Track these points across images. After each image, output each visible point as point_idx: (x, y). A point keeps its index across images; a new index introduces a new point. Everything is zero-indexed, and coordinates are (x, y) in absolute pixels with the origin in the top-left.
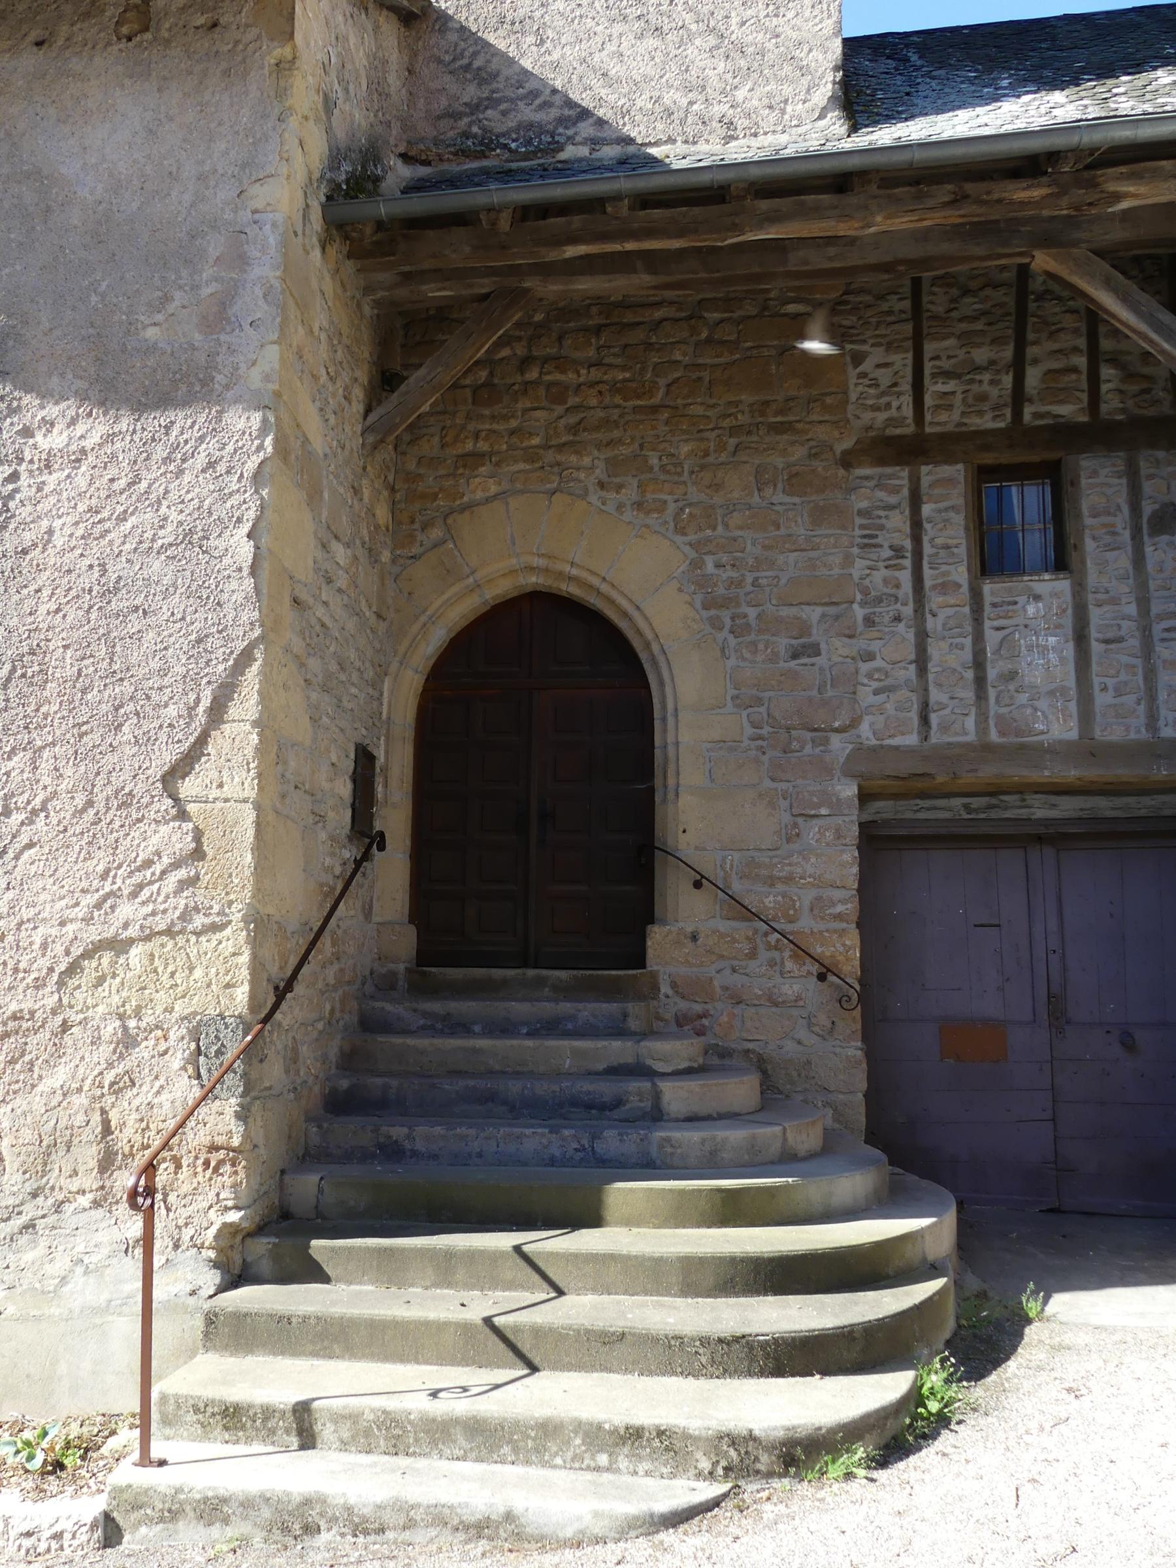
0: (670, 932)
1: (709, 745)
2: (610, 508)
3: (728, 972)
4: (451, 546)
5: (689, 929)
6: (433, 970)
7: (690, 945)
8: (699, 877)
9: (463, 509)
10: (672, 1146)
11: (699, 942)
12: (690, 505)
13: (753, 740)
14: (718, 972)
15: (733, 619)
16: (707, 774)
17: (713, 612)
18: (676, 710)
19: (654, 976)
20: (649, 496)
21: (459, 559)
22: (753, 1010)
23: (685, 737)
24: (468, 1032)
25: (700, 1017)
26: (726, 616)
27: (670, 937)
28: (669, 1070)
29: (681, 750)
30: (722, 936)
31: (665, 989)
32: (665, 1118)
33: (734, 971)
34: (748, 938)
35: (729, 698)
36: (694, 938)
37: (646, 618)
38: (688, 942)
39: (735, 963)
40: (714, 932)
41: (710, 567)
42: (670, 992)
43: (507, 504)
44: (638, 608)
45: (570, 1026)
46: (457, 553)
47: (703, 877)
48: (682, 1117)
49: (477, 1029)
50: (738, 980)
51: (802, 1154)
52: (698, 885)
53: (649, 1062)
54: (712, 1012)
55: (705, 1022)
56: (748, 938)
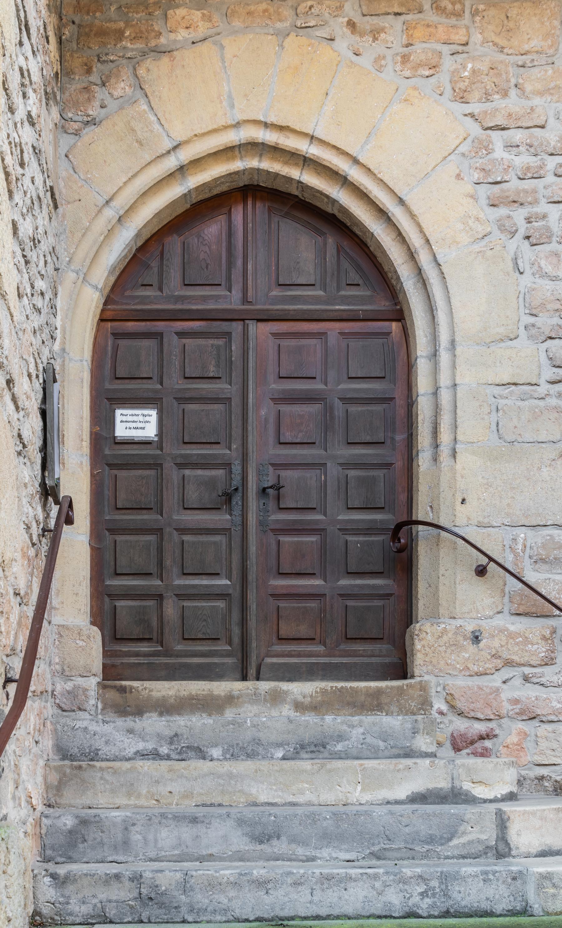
0: (445, 631)
1: (497, 391)
2: (366, 61)
3: (518, 681)
4: (145, 107)
5: (470, 627)
6: (135, 684)
7: (472, 648)
8: (485, 560)
9: (159, 52)
10: (554, 886)
11: (482, 644)
12: (474, 59)
13: (553, 383)
14: (504, 682)
15: (528, 220)
16: (494, 427)
17: (503, 211)
18: (453, 343)
19: (423, 687)
20: (418, 47)
21: (157, 126)
22: (550, 727)
23: (467, 377)
24: (204, 758)
25: (482, 738)
26: (519, 215)
27: (445, 638)
28: (491, 796)
29: (459, 395)
30: (511, 636)
31: (439, 704)
32: (513, 853)
33: (526, 679)
34: (544, 638)
35: (522, 328)
36: (476, 638)
37: (412, 216)
38: (467, 643)
39: (527, 670)
40: (501, 631)
41: (499, 153)
42: (444, 708)
43: (222, 47)
44: (401, 202)
45: (339, 747)
46: (153, 118)
47: (491, 559)
48: (534, 851)
49: (216, 752)
50: (530, 693)
51: (498, 913)
52: (481, 571)
53: (467, 786)
54: (497, 732)
55: (488, 743)
56: (544, 638)
